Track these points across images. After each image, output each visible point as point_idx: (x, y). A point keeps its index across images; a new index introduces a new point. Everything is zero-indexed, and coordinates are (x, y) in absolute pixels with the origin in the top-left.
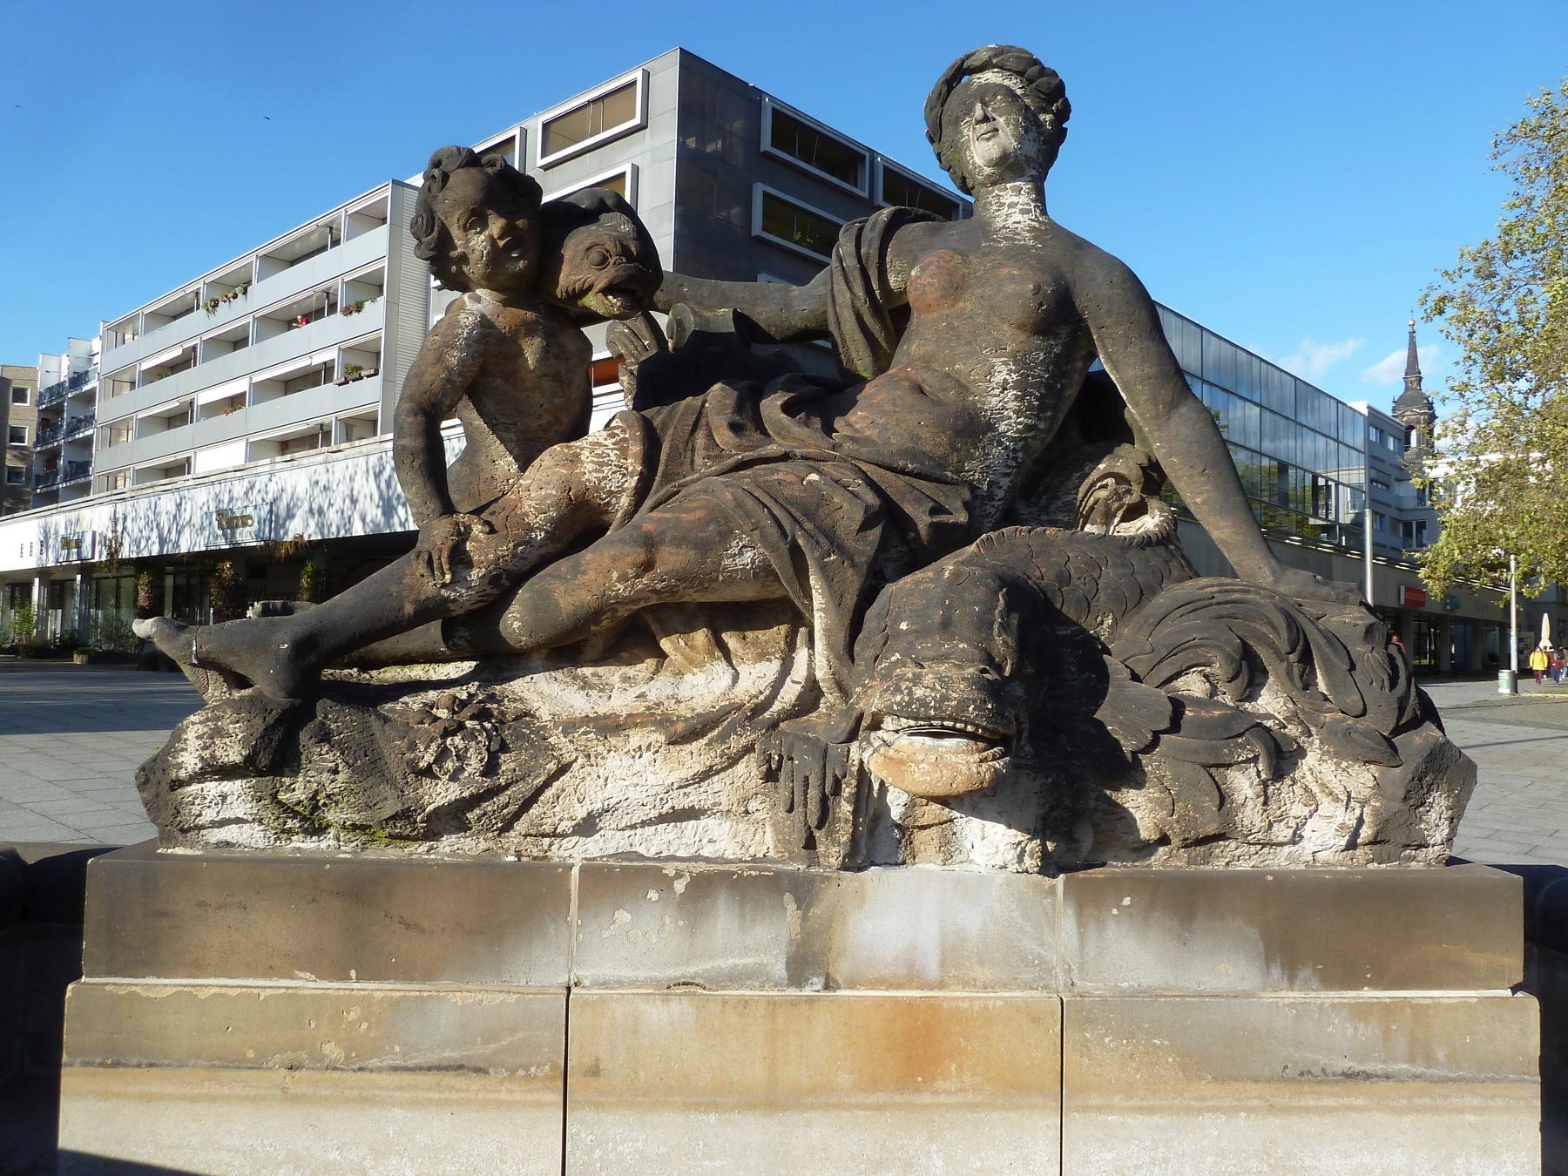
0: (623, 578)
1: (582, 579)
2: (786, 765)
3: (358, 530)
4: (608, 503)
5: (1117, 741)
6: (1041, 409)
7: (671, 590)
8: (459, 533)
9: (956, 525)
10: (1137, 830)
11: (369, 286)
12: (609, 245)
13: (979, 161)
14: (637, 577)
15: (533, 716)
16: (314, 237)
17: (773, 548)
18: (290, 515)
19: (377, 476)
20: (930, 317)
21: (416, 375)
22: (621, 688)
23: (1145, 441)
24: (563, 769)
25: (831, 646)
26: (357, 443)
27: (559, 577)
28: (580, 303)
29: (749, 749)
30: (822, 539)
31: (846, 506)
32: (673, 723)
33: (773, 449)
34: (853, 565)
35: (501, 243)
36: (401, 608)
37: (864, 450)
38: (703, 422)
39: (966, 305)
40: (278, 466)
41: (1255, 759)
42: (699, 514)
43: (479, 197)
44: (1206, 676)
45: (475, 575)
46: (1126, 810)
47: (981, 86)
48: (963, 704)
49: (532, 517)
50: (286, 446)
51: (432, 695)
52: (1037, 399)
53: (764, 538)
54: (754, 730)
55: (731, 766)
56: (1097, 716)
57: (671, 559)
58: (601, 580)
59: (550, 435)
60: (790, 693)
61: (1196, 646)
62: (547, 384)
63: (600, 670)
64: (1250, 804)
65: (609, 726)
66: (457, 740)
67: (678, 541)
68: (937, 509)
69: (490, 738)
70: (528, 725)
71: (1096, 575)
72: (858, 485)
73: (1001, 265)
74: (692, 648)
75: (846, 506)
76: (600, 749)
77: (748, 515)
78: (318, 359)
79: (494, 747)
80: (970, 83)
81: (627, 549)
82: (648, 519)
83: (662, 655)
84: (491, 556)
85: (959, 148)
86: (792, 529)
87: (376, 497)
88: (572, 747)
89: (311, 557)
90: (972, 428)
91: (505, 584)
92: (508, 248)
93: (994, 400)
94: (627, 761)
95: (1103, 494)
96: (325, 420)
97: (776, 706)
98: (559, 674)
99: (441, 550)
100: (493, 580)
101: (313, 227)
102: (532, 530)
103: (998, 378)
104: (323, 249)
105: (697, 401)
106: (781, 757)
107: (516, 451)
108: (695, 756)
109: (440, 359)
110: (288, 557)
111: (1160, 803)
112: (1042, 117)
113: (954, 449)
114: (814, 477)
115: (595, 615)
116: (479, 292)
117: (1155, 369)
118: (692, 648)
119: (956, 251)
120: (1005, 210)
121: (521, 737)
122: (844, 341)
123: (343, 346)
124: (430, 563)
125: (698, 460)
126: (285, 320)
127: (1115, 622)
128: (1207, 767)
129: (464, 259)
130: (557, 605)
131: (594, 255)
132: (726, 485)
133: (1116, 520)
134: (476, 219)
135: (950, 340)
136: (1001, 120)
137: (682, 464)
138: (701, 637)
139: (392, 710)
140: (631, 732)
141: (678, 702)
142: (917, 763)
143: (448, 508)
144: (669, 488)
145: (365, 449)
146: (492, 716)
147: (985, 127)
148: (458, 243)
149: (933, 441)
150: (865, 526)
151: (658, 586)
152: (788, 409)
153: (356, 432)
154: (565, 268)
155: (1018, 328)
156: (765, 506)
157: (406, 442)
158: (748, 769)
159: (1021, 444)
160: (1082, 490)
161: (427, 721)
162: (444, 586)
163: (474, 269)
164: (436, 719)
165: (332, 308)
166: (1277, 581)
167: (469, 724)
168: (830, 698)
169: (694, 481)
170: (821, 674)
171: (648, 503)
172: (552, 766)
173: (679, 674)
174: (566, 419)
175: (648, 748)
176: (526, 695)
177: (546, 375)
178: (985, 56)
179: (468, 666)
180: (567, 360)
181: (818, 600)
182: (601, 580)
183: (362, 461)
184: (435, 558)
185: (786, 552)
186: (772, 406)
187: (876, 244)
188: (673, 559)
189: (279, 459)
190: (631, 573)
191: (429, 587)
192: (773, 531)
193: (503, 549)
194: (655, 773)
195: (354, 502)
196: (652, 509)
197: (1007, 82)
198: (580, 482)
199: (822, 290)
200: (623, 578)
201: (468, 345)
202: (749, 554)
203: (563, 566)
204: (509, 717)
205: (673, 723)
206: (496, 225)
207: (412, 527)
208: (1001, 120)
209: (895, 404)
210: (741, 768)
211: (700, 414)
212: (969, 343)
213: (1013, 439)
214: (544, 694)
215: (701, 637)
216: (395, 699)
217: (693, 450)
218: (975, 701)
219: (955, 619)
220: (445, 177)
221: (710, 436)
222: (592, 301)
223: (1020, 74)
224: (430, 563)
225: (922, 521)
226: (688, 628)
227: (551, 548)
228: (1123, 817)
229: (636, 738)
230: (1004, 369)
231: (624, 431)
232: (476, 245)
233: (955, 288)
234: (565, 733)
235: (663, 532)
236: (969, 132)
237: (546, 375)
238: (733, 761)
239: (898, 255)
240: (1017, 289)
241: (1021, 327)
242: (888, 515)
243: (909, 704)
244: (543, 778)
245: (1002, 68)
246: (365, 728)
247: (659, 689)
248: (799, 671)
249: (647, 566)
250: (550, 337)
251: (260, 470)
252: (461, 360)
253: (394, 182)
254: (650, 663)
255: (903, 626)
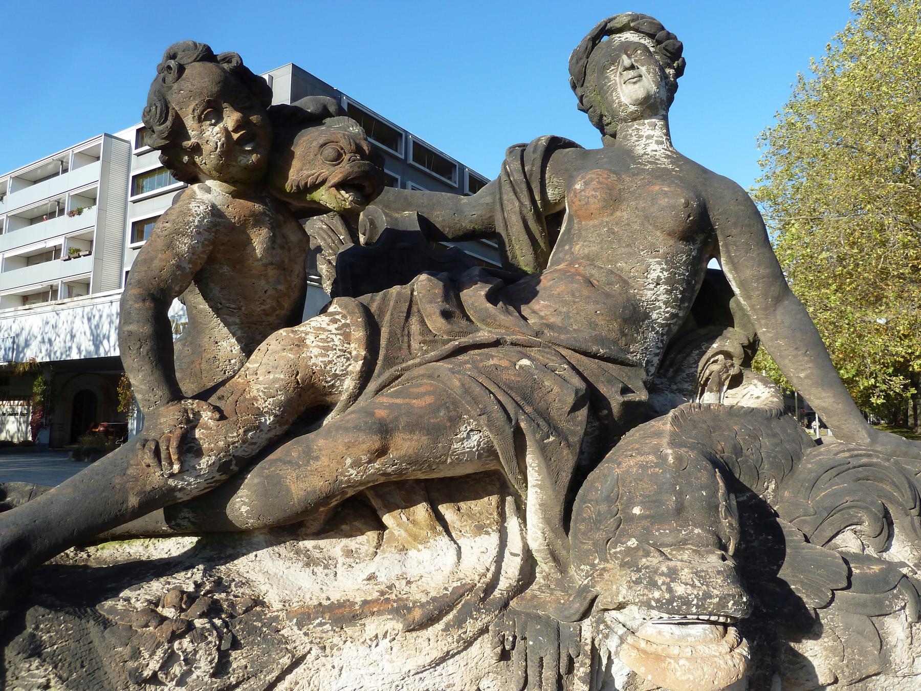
0: (356, 464)
1: (314, 465)
2: (520, 644)
3: (75, 356)
4: (333, 386)
5: (800, 599)
6: (682, 300)
7: (400, 472)
8: (188, 421)
9: (640, 403)
10: (816, 676)
11: (88, 198)
12: (343, 143)
13: (625, 100)
14: (370, 462)
15: (263, 604)
16: (50, 167)
17: (499, 432)
18: (27, 345)
19: (89, 319)
20: (591, 223)
21: (145, 261)
22: (348, 567)
23: (747, 323)
24: (297, 662)
25: (547, 520)
26: (75, 299)
27: (290, 462)
28: (309, 197)
29: (484, 631)
30: (542, 422)
31: (556, 389)
32: (409, 610)
33: (484, 334)
34: (569, 445)
35: (235, 136)
36: (125, 501)
37: (563, 337)
38: (414, 309)
39: (623, 214)
40: (19, 313)
41: (904, 608)
42: (429, 400)
43: (215, 89)
44: (855, 532)
45: (204, 463)
46: (805, 658)
47: (622, 44)
48: (724, 599)
49: (261, 401)
50: (26, 299)
51: (156, 587)
52: (681, 293)
53: (491, 424)
54: (488, 611)
55: (465, 649)
56: (781, 575)
57: (404, 445)
58: (334, 465)
59: (271, 319)
60: (512, 568)
61: (849, 507)
62: (271, 272)
63: (322, 543)
64: (900, 645)
65: (344, 615)
66: (186, 642)
67: (412, 428)
68: (625, 390)
69: (220, 637)
70: (259, 616)
71: (758, 446)
72: (564, 370)
73: (650, 183)
74: (414, 522)
75: (556, 389)
76: (336, 640)
77: (475, 401)
78: (50, 244)
79: (225, 645)
80: (610, 42)
81: (362, 437)
82: (382, 404)
83: (382, 527)
84: (221, 444)
85: (603, 90)
86: (516, 414)
87: (88, 333)
88: (306, 639)
89: (41, 373)
90: (634, 316)
91: (234, 470)
92: (242, 141)
93: (649, 293)
94: (363, 650)
95: (715, 367)
96: (54, 283)
97: (504, 584)
98: (281, 549)
99: (169, 440)
100: (223, 467)
101: (50, 160)
102: (260, 414)
103: (653, 275)
104: (57, 174)
105: (405, 289)
106: (515, 637)
107: (239, 333)
108: (433, 642)
109: (170, 246)
110: (25, 373)
111: (833, 650)
112: (668, 71)
113: (624, 334)
114: (525, 362)
115: (328, 498)
116: (209, 183)
117: (768, 271)
118: (414, 522)
119: (610, 171)
120: (644, 141)
121: (252, 631)
122: (510, 240)
123: (69, 236)
124: (157, 453)
125: (415, 345)
126: (33, 218)
127: (777, 487)
128: (870, 616)
129: (197, 149)
130: (288, 490)
131: (329, 151)
132: (452, 371)
133: (725, 388)
134: (212, 111)
135: (611, 242)
136: (643, 69)
137: (400, 348)
138: (421, 511)
139: (113, 610)
140: (367, 621)
141: (409, 583)
142: (677, 658)
143: (176, 395)
144: (392, 371)
145: (81, 303)
146: (221, 610)
147: (631, 73)
148: (192, 133)
149: (608, 327)
150: (575, 408)
151: (389, 470)
152: (492, 298)
153: (75, 291)
154: (296, 164)
155: (669, 234)
156: (491, 392)
157: (133, 327)
158: (484, 651)
159: (666, 329)
160: (701, 364)
161: (153, 623)
162: (172, 475)
163: (207, 160)
164: (163, 619)
165: (61, 212)
166: (874, 441)
167: (198, 623)
168: (544, 567)
169: (416, 366)
170: (536, 543)
171: (372, 386)
172: (286, 661)
173: (403, 549)
174: (287, 304)
175: (385, 636)
176: (252, 576)
177: (272, 264)
178: (625, 20)
179: (188, 542)
180: (289, 250)
181: (533, 476)
182: (334, 465)
183: (79, 311)
184: (163, 448)
185: (510, 436)
186: (475, 296)
187: (538, 163)
188: (406, 445)
189: (20, 308)
190: (364, 458)
191: (156, 478)
192: (499, 416)
193: (233, 436)
194: (391, 661)
195: (73, 337)
196: (378, 391)
197: (642, 41)
198: (307, 366)
199: (488, 199)
200: (356, 464)
201: (199, 233)
202: (475, 437)
203: (292, 449)
204: (240, 609)
205: (409, 610)
206: (231, 119)
207: (117, 353)
208: (643, 69)
209: (573, 295)
210: (475, 649)
211: (411, 301)
212: (628, 246)
213: (662, 325)
214: (271, 575)
215: (421, 511)
216: (114, 593)
217: (409, 335)
218: (734, 596)
219: (686, 504)
220: (181, 69)
221: (422, 322)
222: (323, 196)
223: (652, 36)
224: (157, 453)
225: (616, 401)
226: (409, 503)
227: (279, 431)
228: (803, 665)
229: (373, 626)
230: (658, 268)
231: (344, 317)
232: (210, 136)
233: (613, 200)
234: (300, 625)
235: (397, 419)
236: (615, 76)
237: (272, 264)
238: (469, 644)
239: (556, 173)
240: (671, 204)
241: (671, 234)
242: (591, 398)
243: (670, 602)
244: (275, 674)
245: (637, 30)
246: (82, 636)
247: (386, 566)
248: (514, 544)
249: (382, 452)
250: (275, 228)
251: (7, 315)
252: (192, 248)
253: (106, 135)
254: (372, 535)
255: (637, 511)
